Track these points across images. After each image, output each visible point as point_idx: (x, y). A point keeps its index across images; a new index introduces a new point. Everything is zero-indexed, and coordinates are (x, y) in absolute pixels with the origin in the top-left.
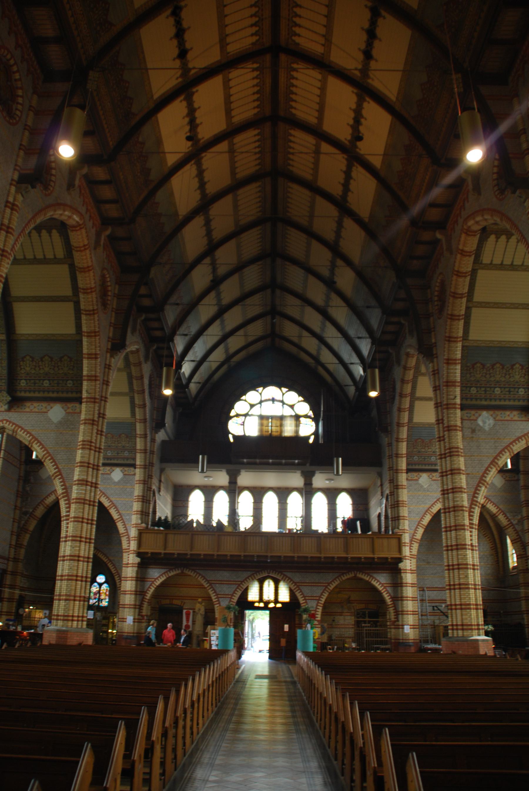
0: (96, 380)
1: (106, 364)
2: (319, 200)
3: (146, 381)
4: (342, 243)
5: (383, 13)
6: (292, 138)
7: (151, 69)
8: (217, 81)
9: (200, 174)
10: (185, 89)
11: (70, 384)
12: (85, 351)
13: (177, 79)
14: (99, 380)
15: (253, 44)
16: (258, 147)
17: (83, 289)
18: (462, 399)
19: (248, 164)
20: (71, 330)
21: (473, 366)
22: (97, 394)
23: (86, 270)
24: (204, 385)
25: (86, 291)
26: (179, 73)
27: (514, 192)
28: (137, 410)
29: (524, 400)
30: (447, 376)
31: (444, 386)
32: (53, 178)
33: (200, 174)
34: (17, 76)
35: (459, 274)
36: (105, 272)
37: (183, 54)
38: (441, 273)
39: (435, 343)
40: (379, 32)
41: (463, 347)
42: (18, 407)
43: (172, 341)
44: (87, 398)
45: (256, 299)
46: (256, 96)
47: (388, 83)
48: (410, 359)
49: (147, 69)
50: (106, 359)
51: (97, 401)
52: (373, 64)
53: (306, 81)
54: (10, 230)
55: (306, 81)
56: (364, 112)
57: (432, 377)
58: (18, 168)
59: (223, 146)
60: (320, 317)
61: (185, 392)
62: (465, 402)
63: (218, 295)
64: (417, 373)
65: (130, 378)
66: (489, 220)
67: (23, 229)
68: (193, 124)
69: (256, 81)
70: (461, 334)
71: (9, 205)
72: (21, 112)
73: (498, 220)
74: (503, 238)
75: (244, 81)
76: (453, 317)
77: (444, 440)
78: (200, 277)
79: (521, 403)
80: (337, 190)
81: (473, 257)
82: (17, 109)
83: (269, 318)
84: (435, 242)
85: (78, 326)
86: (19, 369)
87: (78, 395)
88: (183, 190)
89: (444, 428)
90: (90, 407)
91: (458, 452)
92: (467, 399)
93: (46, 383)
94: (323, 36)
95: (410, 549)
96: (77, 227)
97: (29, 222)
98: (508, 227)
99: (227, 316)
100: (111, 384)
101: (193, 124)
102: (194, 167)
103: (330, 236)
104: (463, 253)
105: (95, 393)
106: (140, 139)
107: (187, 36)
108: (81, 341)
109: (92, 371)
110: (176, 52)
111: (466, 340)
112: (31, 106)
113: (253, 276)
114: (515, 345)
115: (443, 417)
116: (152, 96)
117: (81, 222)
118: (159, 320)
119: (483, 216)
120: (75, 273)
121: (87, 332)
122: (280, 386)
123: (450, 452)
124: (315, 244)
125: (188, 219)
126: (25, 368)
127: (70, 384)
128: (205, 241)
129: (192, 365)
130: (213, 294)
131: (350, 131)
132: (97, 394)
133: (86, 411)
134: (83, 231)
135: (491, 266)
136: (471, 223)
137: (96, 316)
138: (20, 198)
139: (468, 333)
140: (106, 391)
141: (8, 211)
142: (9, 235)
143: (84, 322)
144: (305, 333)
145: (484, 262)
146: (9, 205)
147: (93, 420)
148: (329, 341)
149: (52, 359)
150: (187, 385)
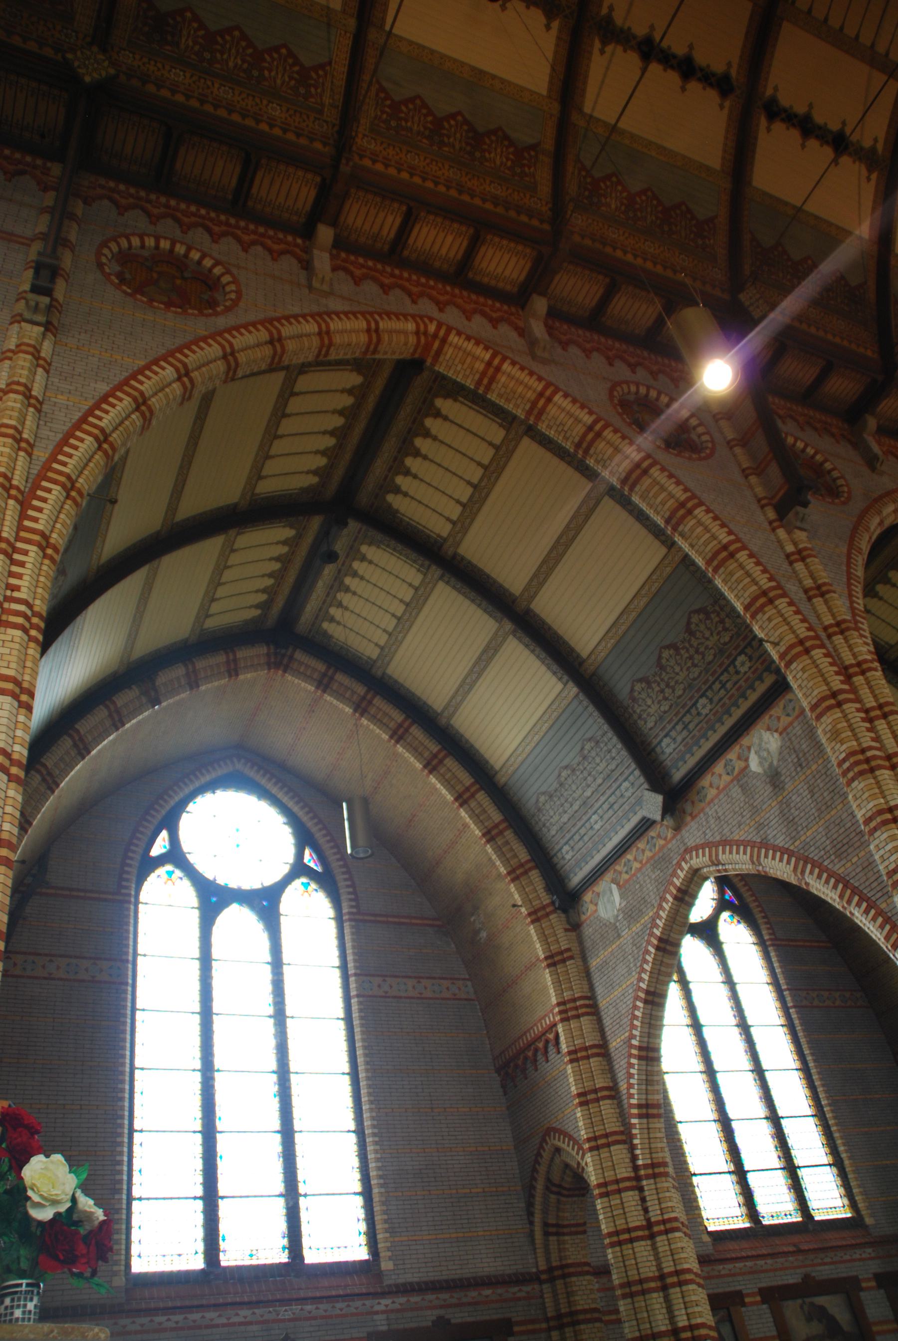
7: (618, 120)
11: (743, 664)
13: (869, 179)
32: (835, 474)
49: (799, 210)
54: (824, 589)
58: (763, 502)
67: (849, 573)
71: (792, 558)
72: (708, 433)
82: (699, 436)
97: (849, 557)
126: (650, 712)
138: (801, 535)
141: (799, 566)
142: (827, 596)
146: (792, 558)
149: (673, 646)
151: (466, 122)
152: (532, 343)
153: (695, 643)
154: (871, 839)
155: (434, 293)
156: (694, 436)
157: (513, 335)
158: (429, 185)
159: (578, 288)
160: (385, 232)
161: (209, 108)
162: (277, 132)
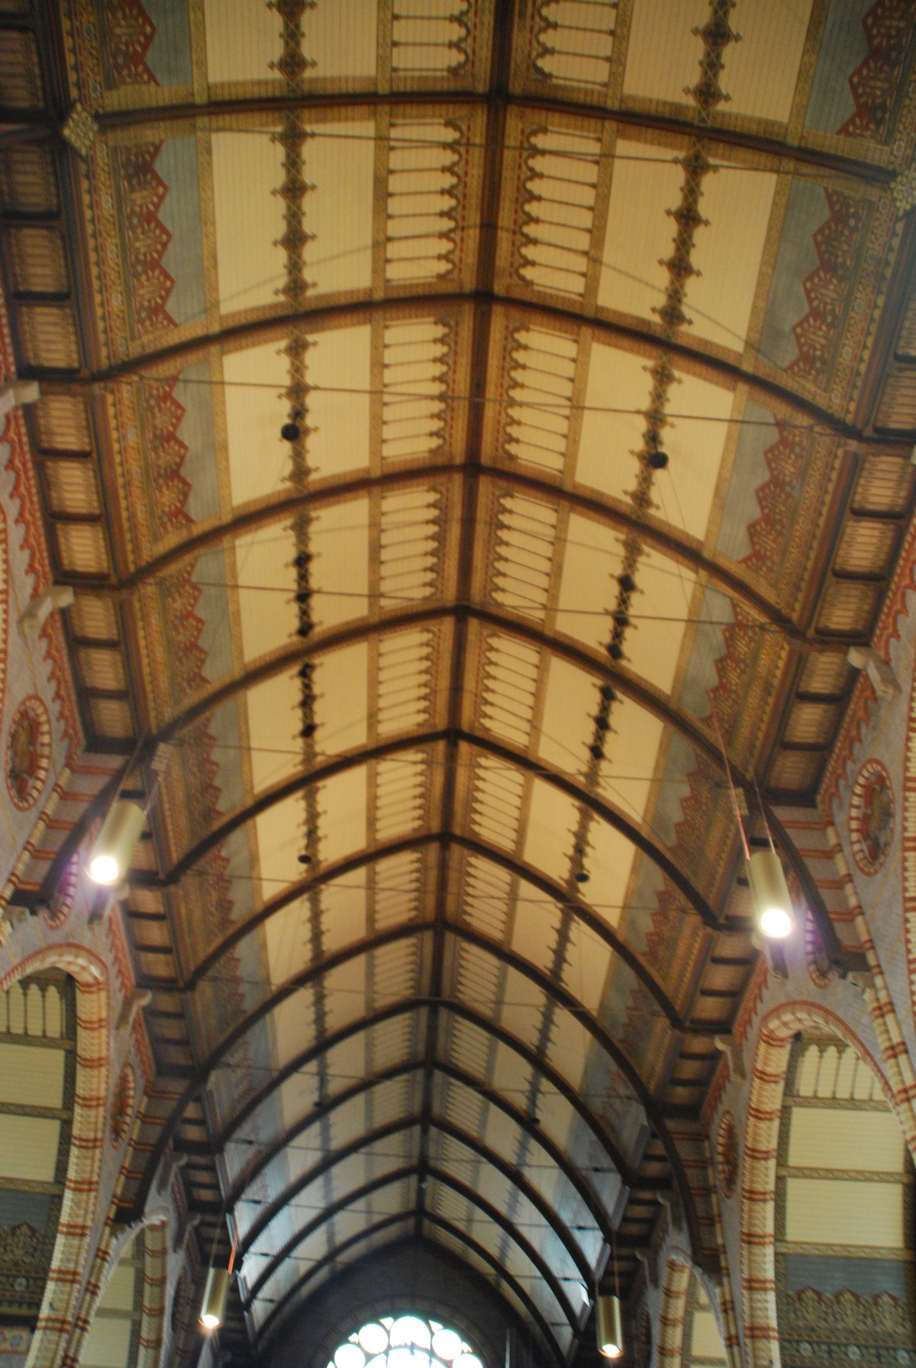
0: (73, 1281)
1: (99, 1249)
2: (513, 973)
3: (170, 1290)
5: (619, 695)
6: (471, 870)
8: (357, 775)
9: (316, 916)
10: (307, 781)
12: (64, 1218)
14: (80, 1282)
15: (419, 725)
16: (417, 880)
17: (84, 1099)
19: (396, 908)
20: (47, 1174)
21: (799, 1295)
23: (94, 1064)
24: (280, 1305)
25: (88, 1103)
26: (299, 758)
27: (843, 976)
28: (142, 1351)
30: (752, 1316)
33: (316, 916)
34: (46, 739)
35: (759, 1115)
36: (129, 1071)
37: (308, 730)
40: (613, 720)
41: (776, 1254)
43: (231, 1210)
44: (48, 1320)
46: (419, 802)
47: (629, 792)
48: (677, 1275)
49: (249, 749)
50: (101, 1238)
51: (67, 1327)
52: (604, 766)
53: (497, 783)
55: (497, 783)
56: (591, 837)
57: (721, 1316)
59: (358, 875)
60: (508, 1184)
61: (242, 1319)
63: (326, 1130)
64: (692, 1304)
65: (140, 1279)
66: (806, 1020)
68: (312, 836)
69: (420, 779)
70: (770, 1228)
73: (821, 1021)
74: (832, 1051)
75: (402, 776)
76: (753, 1196)
78: (296, 1096)
80: (544, 960)
81: (782, 1084)
84: (714, 1056)
85: (61, 1168)
87: (32, 1312)
88: (284, 943)
90: (50, 1341)
94: (529, 721)
96: (92, 987)
98: (839, 1034)
99: (336, 1170)
100: (101, 1293)
101: (312, 836)
102: (307, 905)
103: (530, 1038)
104: (764, 1076)
105: (66, 1311)
106: (224, 854)
107: (318, 706)
108: (60, 1197)
109: (68, 1260)
110: (299, 726)
112: (57, 785)
113: (391, 1100)
114: (877, 1255)
116: (252, 788)
117: (101, 979)
118: (211, 1168)
119: (793, 1013)
120: (75, 1068)
121: (76, 1182)
122: (427, 1315)
124: (503, 1049)
125: (286, 992)
129: (264, 1262)
130: (316, 1128)
131: (567, 864)
132: (71, 1310)
133: (40, 1350)
134: (103, 994)
135: (815, 1101)
136: (774, 1024)
137: (98, 1151)
140: (90, 1306)
143: (73, 1160)
144: (480, 1214)
148: (525, 1231)
150: (248, 1305)
151: (182, 458)
152: (30, 613)
155: (28, 505)
156: (31, 782)
157: (29, 590)
158: (117, 459)
159: (97, 617)
160: (58, 439)
161: (91, 243)
162: (99, 312)
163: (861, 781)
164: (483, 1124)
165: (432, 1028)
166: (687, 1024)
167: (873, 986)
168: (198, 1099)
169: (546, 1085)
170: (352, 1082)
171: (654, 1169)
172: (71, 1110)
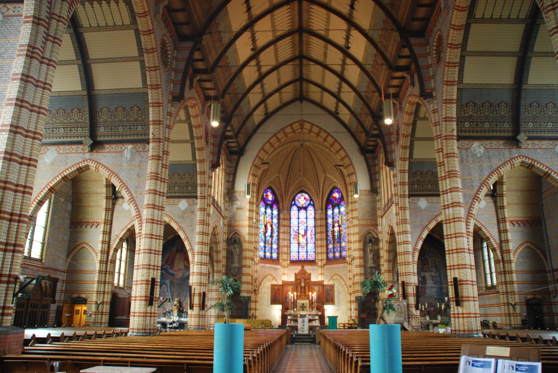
2: (333, 16)
4: (346, 73)
10: (249, 26)
18: (458, 131)
20: (190, 158)
22: (206, 194)
29: (508, 132)
31: (443, 121)
37: (249, 9)
38: (438, 30)
39: (434, 88)
41: (458, 89)
42: (99, 149)
45: (290, 88)
62: (460, 134)
77: (444, 165)
78: (254, 98)
79: (506, 134)
83: (298, 83)
86: (98, 118)
87: (147, 137)
88: (249, 75)
89: (443, 155)
91: (456, 174)
92: (462, 131)
93: (121, 129)
95: (467, 225)
105: (160, 134)
108: (196, 164)
110: (246, 9)
111: (460, 83)
115: (443, 146)
123: (449, 175)
126: (102, 117)
127: (190, 188)
128: (257, 74)
130: (259, 86)
135: (483, 20)
139: (462, 77)
145: (476, 17)
147: (159, 157)
153: (130, 113)
154: (11, 82)
163: (436, 37)
164: (325, 55)
165: (301, 88)
166: (394, 67)
167: (433, 103)
168: (199, 50)
169: (349, 61)
170: (277, 114)
171: (403, 62)
172: (143, 56)
